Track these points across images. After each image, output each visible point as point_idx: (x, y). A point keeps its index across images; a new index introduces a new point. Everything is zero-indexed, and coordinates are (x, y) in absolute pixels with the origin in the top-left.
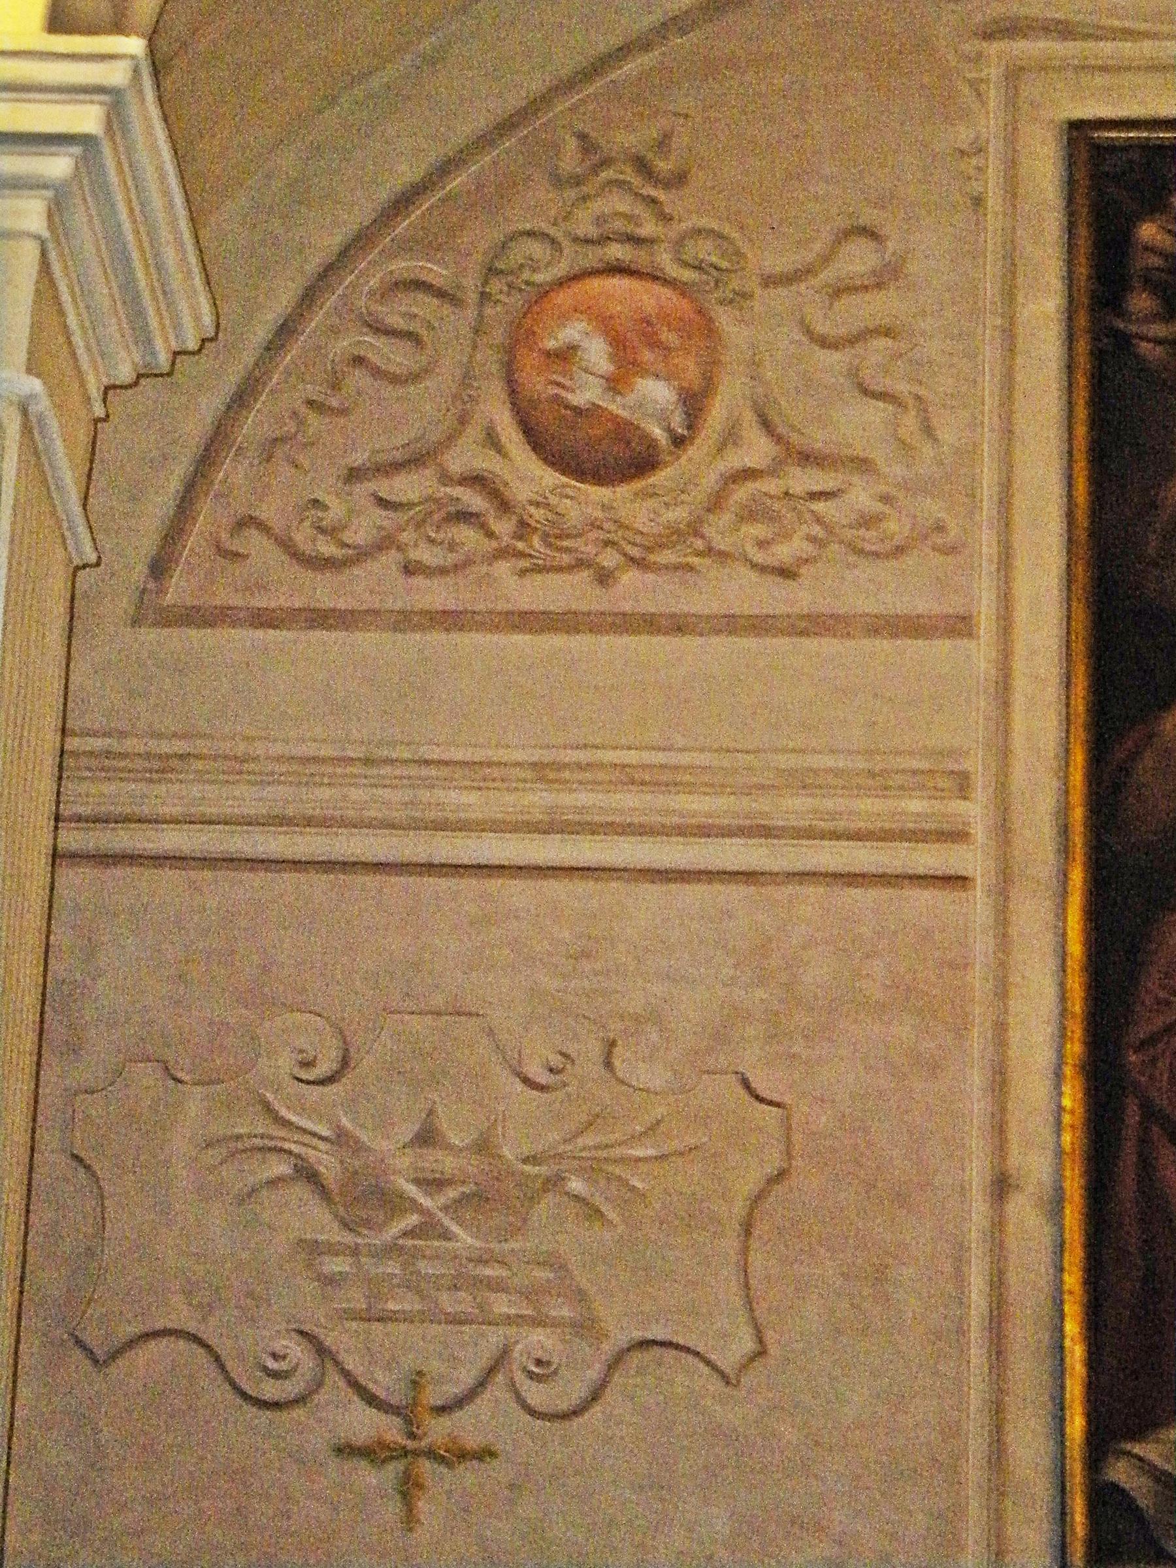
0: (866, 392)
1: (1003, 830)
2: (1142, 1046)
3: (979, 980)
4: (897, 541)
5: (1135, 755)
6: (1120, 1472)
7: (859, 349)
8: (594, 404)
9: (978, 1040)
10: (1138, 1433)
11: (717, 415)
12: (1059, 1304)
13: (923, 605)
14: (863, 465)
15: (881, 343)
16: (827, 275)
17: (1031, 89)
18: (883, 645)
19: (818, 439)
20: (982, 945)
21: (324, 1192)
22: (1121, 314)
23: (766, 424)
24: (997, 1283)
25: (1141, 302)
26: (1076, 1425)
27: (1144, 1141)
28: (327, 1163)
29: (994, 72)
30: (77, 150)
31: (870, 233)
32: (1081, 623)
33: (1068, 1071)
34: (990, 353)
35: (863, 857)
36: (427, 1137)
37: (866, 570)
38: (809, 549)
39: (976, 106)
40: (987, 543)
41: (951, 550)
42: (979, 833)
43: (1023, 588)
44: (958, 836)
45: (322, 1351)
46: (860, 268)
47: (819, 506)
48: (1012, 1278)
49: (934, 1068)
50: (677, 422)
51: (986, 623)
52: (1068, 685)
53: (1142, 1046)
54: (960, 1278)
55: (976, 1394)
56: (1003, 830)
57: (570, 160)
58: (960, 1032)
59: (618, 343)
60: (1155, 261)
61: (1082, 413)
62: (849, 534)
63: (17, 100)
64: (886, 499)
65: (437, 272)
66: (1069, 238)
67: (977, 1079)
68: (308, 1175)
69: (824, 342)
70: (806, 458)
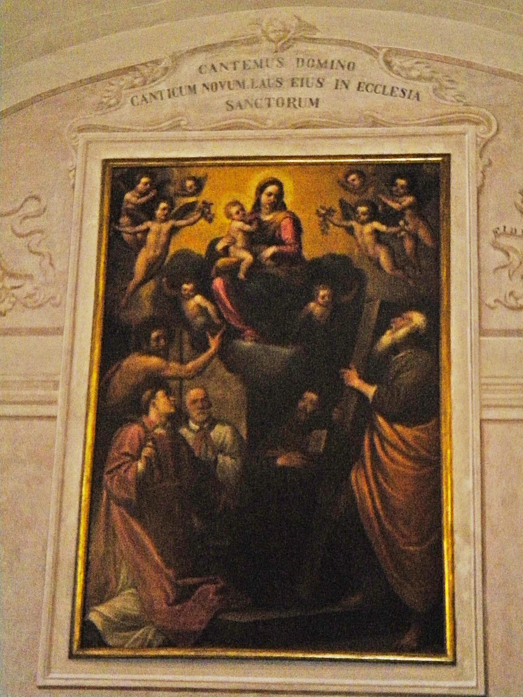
0: (31, 252)
1: (68, 402)
2: (109, 473)
3: (57, 451)
4: (39, 302)
5: (114, 373)
6: (93, 617)
7: (29, 238)
8: (366, 247)
9: (55, 473)
10: (101, 602)
12: (76, 564)
13: (46, 323)
14: (30, 277)
15: (39, 235)
16: (20, 213)
17: (92, 147)
18: (33, 339)
19: (15, 268)
20: (59, 439)
22: (118, 224)
24: (57, 554)
25: (124, 220)
26: (79, 601)
27: (108, 504)
29: (81, 142)
31: (37, 198)
32: (99, 330)
33: (84, 482)
34: (74, 239)
35: (21, 410)
37: (28, 312)
38: (10, 306)
39: (73, 153)
40: (69, 301)
41: (57, 305)
42: (60, 401)
44: (52, 402)
46: (32, 210)
47: (15, 291)
49: (41, 481)
51: (67, 332)
52: (143, 141)
53: (109, 473)
54: (44, 550)
56: (68, 402)
58: (50, 467)
60: (130, 206)
61: (103, 259)
62: (23, 301)
64: (36, 289)
67: (54, 485)
69: (20, 236)
70: (12, 275)
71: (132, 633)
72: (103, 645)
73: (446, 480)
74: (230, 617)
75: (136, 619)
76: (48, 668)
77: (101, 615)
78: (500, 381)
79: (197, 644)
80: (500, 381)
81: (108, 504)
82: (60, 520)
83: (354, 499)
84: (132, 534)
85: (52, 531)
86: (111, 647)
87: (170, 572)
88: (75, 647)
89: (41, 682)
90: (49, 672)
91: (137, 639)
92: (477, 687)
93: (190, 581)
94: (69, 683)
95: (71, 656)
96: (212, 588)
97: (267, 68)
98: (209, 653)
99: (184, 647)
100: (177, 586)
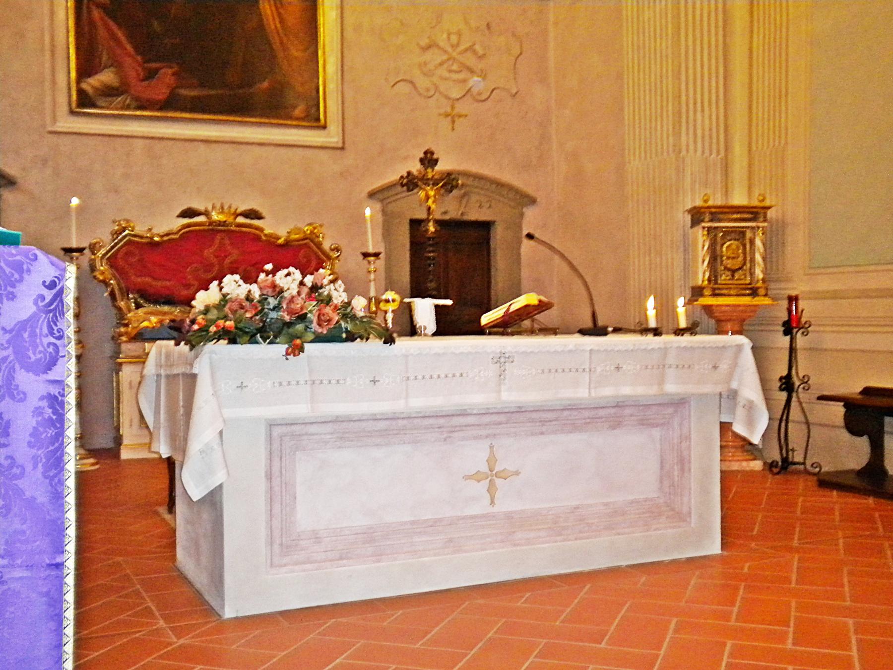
6: (84, 86)
10: (89, 76)
71: (115, 98)
72: (93, 105)
73: (320, 12)
74: (183, 92)
75: (117, 89)
76: (54, 120)
77: (90, 84)
78: (784, 34)
79: (160, 109)
80: (784, 34)
81: (88, 8)
82: (52, 13)
83: (262, 20)
84: (109, 30)
85: (47, 23)
86: (101, 108)
87: (139, 58)
88: (74, 105)
89: (50, 129)
90: (55, 123)
91: (120, 102)
92: (337, 142)
93: (154, 65)
94: (70, 130)
95: (72, 112)
96: (170, 71)
97: (153, 231)
98: (170, 114)
99: (152, 110)
100: (144, 69)
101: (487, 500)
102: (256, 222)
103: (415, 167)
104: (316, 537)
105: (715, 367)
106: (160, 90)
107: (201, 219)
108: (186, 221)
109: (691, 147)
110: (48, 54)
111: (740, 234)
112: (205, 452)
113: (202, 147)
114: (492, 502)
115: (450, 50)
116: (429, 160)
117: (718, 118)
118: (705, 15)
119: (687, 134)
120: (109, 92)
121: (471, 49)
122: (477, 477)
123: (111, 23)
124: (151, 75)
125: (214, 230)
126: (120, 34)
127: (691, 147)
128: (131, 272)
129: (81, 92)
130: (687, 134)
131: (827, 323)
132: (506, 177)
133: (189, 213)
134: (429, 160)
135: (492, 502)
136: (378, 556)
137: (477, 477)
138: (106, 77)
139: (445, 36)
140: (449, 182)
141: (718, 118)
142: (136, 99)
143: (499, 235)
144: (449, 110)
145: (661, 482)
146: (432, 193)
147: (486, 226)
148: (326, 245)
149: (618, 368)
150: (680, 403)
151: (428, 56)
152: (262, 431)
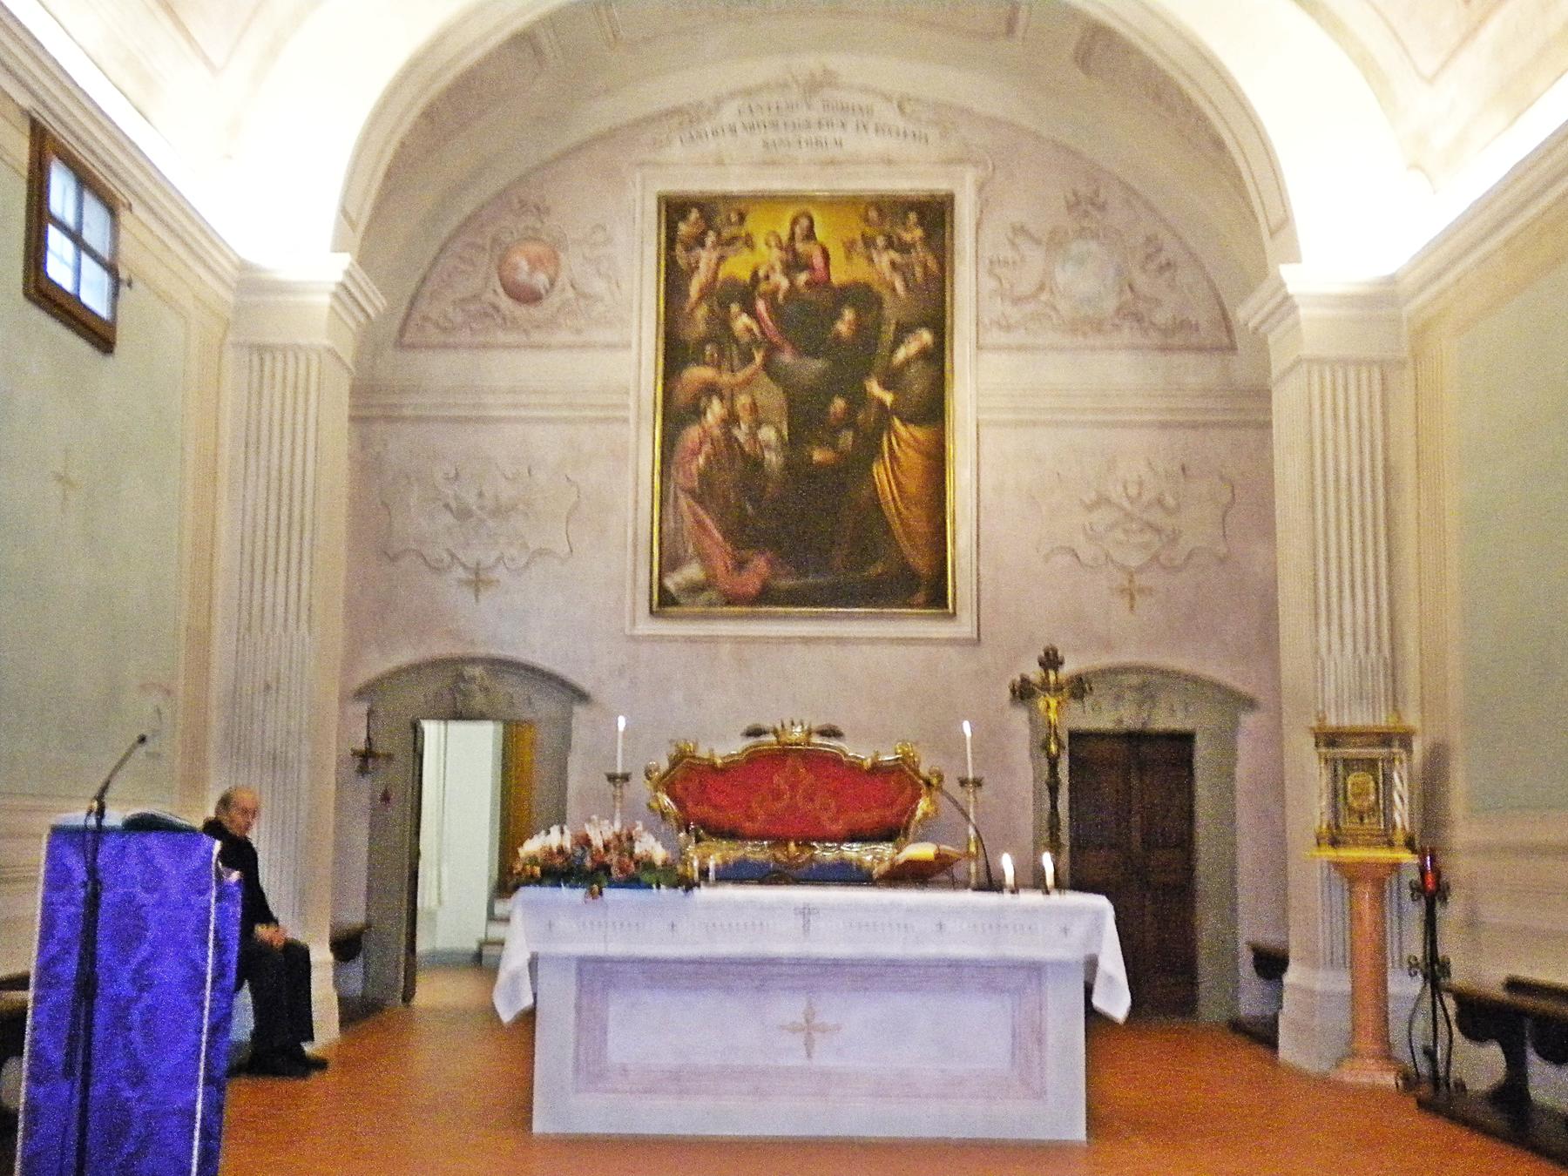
11: (559, 284)
20: (633, 440)
21: (452, 511)
23: (572, 286)
24: (635, 534)
27: (675, 494)
28: (453, 505)
30: (975, 636)
36: (481, 495)
43: (644, 335)
45: (453, 556)
48: (639, 532)
50: (548, 286)
55: (629, 567)
57: (517, 206)
59: (529, 262)
63: (655, 403)
65: (479, 241)
66: (1388, 1036)
68: (447, 506)
76: (634, 623)
101: (804, 1053)
102: (833, 742)
103: (1034, 673)
104: (624, 1070)
105: (1065, 931)
106: (751, 581)
107: (771, 738)
108: (752, 741)
109: (1336, 646)
110: (630, 549)
111: (1371, 764)
112: (515, 978)
113: (799, 649)
114: (809, 1055)
115: (1126, 504)
116: (1051, 661)
117: (1378, 607)
118: (1355, 474)
119: (1329, 625)
120: (695, 589)
121: (1160, 502)
122: (794, 1029)
123: (701, 512)
124: (740, 565)
125: (782, 755)
126: (708, 521)
127: (1336, 646)
128: (690, 804)
129: (663, 590)
130: (1329, 625)
131: (435, 873)
132: (1212, 670)
133: (755, 732)
134: (1051, 661)
135: (809, 1055)
136: (682, 1092)
137: (794, 1029)
138: (692, 572)
139: (1120, 489)
140: (1079, 688)
141: (1378, 607)
142: (725, 593)
143: (1203, 751)
144: (1126, 583)
145: (1013, 1054)
146: (1053, 703)
147: (1184, 740)
148: (924, 770)
149: (941, 926)
150: (1035, 969)
151: (1096, 516)
152: (574, 965)
